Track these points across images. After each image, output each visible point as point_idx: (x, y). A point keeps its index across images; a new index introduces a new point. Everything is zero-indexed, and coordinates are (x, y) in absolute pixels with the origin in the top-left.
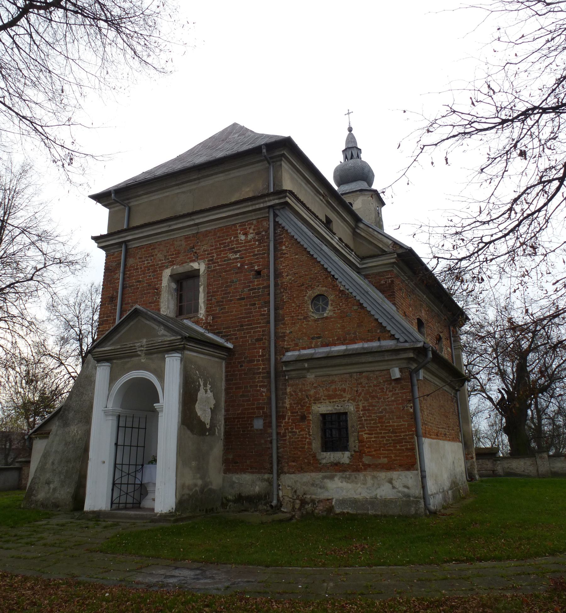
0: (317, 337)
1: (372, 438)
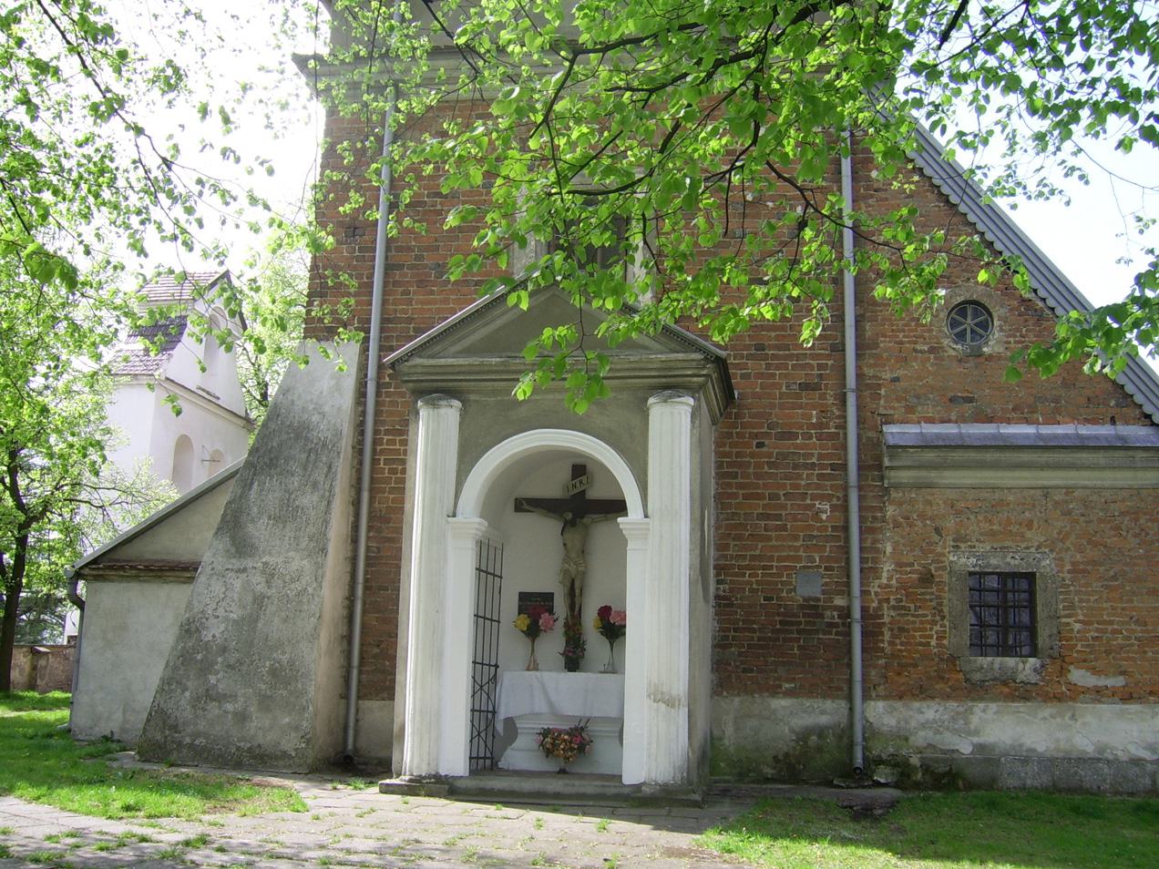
0: (963, 398)
1: (1090, 631)
